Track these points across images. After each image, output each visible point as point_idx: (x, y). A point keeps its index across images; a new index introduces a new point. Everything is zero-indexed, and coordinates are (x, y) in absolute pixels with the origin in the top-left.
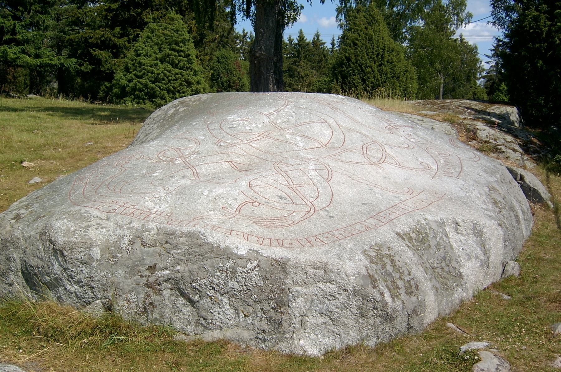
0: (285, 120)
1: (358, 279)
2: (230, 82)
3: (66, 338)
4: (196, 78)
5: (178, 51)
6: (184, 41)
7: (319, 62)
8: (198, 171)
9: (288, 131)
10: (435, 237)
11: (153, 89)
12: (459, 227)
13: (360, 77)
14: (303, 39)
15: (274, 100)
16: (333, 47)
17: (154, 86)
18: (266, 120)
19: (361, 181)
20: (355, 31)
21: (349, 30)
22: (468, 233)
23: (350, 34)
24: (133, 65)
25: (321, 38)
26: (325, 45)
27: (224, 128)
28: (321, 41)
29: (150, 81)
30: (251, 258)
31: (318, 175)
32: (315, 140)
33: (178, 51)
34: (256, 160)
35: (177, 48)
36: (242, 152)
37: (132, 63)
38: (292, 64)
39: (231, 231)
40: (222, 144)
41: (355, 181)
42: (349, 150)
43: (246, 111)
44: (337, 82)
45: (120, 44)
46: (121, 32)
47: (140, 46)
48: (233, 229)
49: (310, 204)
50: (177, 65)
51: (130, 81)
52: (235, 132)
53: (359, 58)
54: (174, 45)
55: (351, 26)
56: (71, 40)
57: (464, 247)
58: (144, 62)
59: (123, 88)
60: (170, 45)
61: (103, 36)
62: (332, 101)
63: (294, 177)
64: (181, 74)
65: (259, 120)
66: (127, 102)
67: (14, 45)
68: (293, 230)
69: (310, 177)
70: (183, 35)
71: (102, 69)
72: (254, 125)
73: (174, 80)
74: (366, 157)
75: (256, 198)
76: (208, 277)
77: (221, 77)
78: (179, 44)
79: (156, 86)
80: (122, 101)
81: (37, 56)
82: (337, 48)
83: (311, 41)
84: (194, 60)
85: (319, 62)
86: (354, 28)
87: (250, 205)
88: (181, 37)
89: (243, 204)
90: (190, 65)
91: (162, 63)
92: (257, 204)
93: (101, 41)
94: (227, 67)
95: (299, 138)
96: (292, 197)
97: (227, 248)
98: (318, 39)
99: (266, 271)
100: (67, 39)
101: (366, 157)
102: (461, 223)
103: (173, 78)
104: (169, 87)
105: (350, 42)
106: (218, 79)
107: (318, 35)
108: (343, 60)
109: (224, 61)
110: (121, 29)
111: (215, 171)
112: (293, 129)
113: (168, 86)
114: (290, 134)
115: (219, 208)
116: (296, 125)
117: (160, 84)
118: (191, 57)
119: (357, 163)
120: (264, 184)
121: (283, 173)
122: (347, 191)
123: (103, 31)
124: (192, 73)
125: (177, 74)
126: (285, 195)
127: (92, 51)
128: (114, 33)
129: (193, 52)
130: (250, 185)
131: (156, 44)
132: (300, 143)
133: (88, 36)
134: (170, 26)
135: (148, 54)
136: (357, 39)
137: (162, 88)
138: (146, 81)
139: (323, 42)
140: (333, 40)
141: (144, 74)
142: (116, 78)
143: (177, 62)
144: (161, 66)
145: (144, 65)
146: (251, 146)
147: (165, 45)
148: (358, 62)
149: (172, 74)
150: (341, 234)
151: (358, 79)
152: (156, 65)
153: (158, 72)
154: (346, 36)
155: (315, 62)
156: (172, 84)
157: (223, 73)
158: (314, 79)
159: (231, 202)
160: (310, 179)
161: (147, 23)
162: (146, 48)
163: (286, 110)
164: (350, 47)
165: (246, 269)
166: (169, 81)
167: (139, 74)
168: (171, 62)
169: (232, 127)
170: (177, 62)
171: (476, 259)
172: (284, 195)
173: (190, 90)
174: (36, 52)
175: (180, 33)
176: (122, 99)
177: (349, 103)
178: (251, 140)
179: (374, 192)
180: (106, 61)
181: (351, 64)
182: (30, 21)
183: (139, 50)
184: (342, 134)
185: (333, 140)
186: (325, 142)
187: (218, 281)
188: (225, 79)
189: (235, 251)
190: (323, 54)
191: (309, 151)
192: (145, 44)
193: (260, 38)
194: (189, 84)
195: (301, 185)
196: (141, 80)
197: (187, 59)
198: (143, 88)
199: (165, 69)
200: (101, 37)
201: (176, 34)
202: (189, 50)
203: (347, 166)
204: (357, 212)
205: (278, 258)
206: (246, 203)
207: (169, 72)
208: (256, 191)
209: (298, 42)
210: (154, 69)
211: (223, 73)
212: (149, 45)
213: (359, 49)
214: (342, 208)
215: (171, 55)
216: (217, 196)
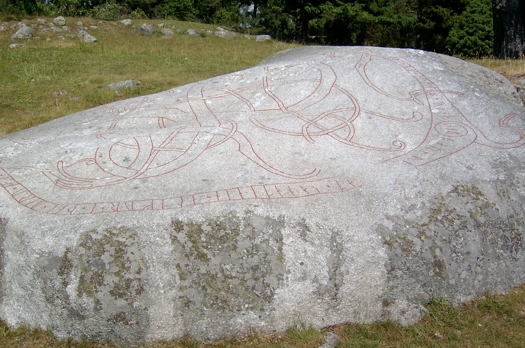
1: (42, 259)
3: (512, 240)
10: (250, 238)
12: (308, 232)
17: (484, 44)
22: (321, 244)
24: (467, 21)
29: (479, 39)
39: (414, 116)
48: (372, 62)
51: (461, 38)
57: (306, 261)
58: (476, 19)
67: (357, 3)
102: (314, 228)
135: (483, 11)
141: (475, 31)
153: (489, 29)
162: (482, 5)
171: (313, 282)
196: (471, 38)
198: (472, 45)
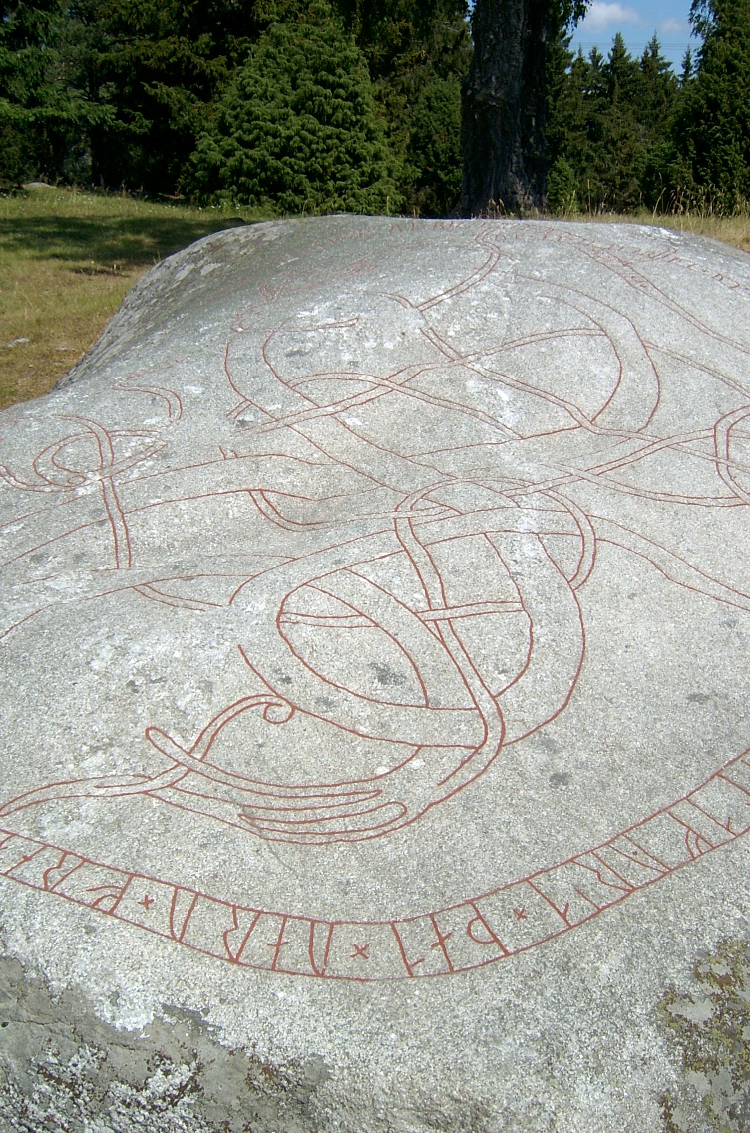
0: (475, 322)
2: (454, 153)
4: (371, 148)
5: (333, 86)
6: (346, 64)
7: (654, 106)
8: (132, 534)
9: (477, 366)
11: (277, 170)
13: (741, 148)
14: (622, 55)
15: (459, 248)
16: (686, 72)
17: (279, 164)
18: (414, 324)
19: (696, 583)
20: (733, 37)
21: (719, 34)
23: (720, 44)
24: (236, 117)
25: (660, 53)
26: (670, 69)
27: (272, 354)
28: (662, 59)
29: (272, 154)
30: (169, 1052)
31: (544, 556)
32: (561, 403)
33: (333, 86)
34: (348, 482)
35: (331, 78)
36: (305, 451)
37: (234, 113)
38: (595, 111)
40: (249, 418)
41: (674, 587)
42: (669, 444)
43: (363, 287)
44: (684, 159)
45: (212, 71)
46: (212, 43)
47: (250, 77)
49: (487, 707)
50: (330, 116)
51: (228, 154)
52: (303, 372)
53: (739, 102)
54: (323, 73)
55: (724, 25)
56: (110, 62)
58: (257, 110)
59: (214, 169)
60: (315, 71)
61: (174, 53)
62: (636, 252)
63: (455, 572)
64: (338, 138)
65: (391, 323)
66: (222, 200)
68: (392, 857)
69: (515, 568)
70: (345, 49)
71: (172, 127)
72: (370, 344)
73: (323, 151)
74: (724, 473)
75: (288, 680)
76: (8, 1091)
77: (435, 141)
78: (334, 70)
79: (285, 163)
80: (212, 197)
81: (33, 102)
82: (695, 76)
83: (640, 60)
84: (367, 105)
85: (654, 106)
86: (729, 30)
87: (253, 717)
88: (340, 55)
89: (230, 713)
90: (358, 117)
91: (298, 114)
92: (287, 709)
93: (169, 66)
94: (448, 120)
95: (504, 395)
96: (425, 672)
97: (73, 993)
98: (655, 54)
99: (229, 1109)
100: (99, 61)
101: (724, 473)
103: (322, 146)
104: (312, 165)
105: (718, 63)
106: (426, 146)
107: (654, 47)
108: (701, 107)
109: (441, 105)
110: (213, 38)
111: (195, 529)
112: (493, 357)
113: (309, 163)
114: (482, 377)
115: (134, 732)
116: (506, 345)
117: (293, 160)
118: (359, 99)
119: (691, 501)
120: (332, 607)
121: (418, 550)
122: (641, 631)
123: (174, 43)
124: (362, 135)
125: (329, 137)
126: (405, 661)
127: (146, 86)
128: (197, 48)
129: (367, 88)
130: (281, 613)
131: (288, 70)
132: (507, 414)
133: (143, 54)
134: (317, 30)
136: (736, 56)
137: (296, 167)
138: (262, 155)
139: (666, 61)
140: (688, 57)
141: (258, 138)
142: (200, 148)
143: (330, 111)
144: (295, 121)
145: (257, 118)
146: (344, 424)
147: (306, 73)
148: (738, 112)
149: (319, 137)
150: (580, 892)
151: (736, 151)
152: (284, 118)
153: (288, 132)
154: (709, 48)
155: (645, 107)
156: (319, 160)
157: (437, 132)
158: (640, 146)
159: (188, 698)
160: (513, 576)
161: (265, 25)
162: (264, 81)
163: (485, 288)
164: (719, 75)
165: (147, 1093)
166: (313, 154)
167: (249, 138)
168: (316, 110)
169: (298, 352)
170: (330, 111)
172: (400, 663)
173: (357, 172)
174: (32, 94)
175: (337, 44)
176: (213, 194)
177: (686, 257)
178: (347, 404)
179: (739, 635)
180: (180, 109)
181: (720, 117)
182: (15, 25)
183: (248, 84)
184: (652, 375)
185: (618, 402)
186: (591, 407)
187: (45, 1114)
188: (444, 146)
189: (106, 1012)
190: (665, 86)
191: (532, 445)
192: (261, 70)
193: (487, 56)
194: (356, 159)
195: (475, 609)
196: (251, 152)
197: (351, 104)
199: (303, 126)
200: (170, 57)
201: (327, 48)
202: (358, 83)
203: (655, 516)
204: (667, 742)
205: (276, 1060)
206: (244, 704)
207: (313, 132)
208: (297, 643)
209: (612, 62)
210: (280, 128)
211: (437, 132)
212: (269, 73)
213: (740, 79)
214: (612, 722)
215: (317, 94)
216: (140, 672)
